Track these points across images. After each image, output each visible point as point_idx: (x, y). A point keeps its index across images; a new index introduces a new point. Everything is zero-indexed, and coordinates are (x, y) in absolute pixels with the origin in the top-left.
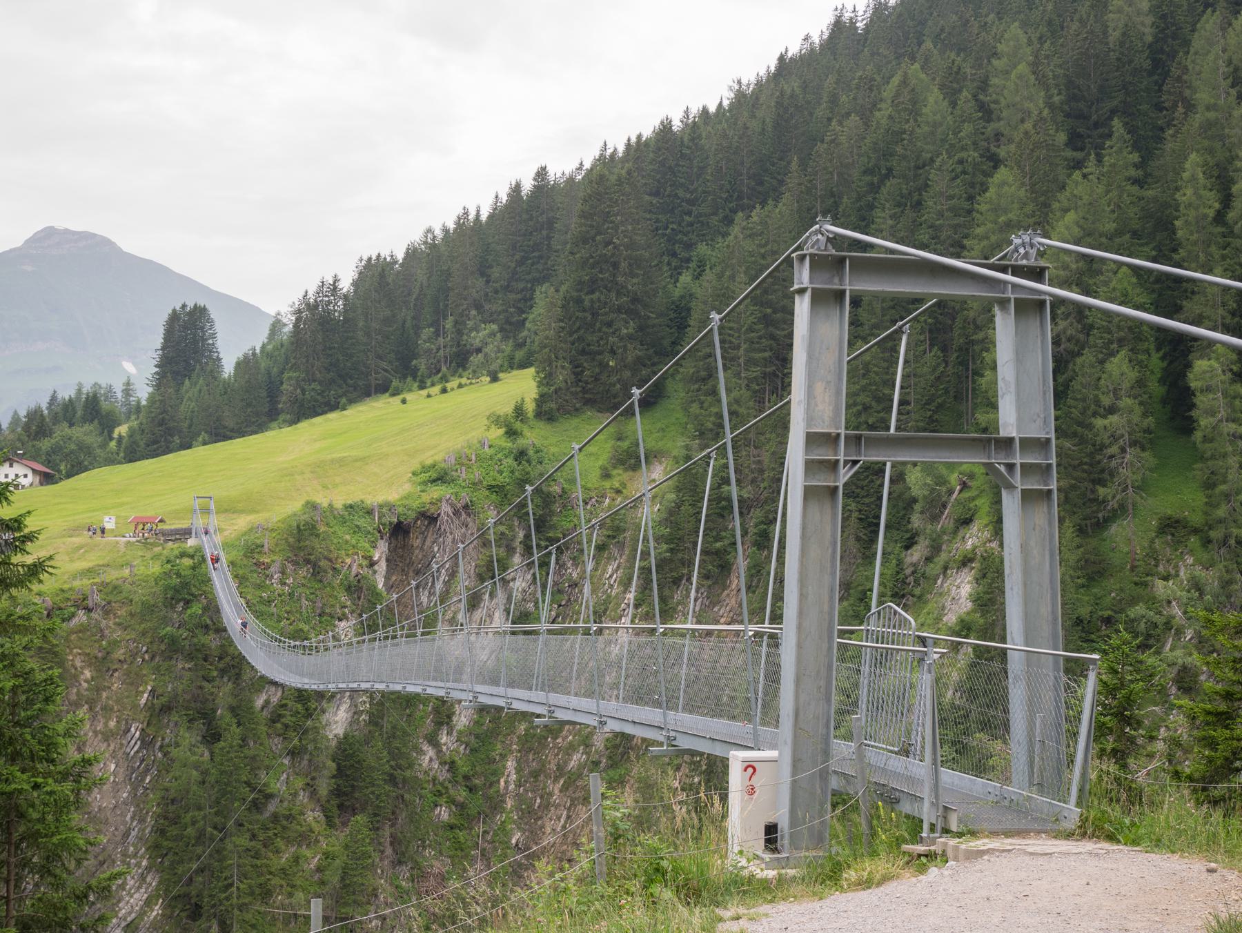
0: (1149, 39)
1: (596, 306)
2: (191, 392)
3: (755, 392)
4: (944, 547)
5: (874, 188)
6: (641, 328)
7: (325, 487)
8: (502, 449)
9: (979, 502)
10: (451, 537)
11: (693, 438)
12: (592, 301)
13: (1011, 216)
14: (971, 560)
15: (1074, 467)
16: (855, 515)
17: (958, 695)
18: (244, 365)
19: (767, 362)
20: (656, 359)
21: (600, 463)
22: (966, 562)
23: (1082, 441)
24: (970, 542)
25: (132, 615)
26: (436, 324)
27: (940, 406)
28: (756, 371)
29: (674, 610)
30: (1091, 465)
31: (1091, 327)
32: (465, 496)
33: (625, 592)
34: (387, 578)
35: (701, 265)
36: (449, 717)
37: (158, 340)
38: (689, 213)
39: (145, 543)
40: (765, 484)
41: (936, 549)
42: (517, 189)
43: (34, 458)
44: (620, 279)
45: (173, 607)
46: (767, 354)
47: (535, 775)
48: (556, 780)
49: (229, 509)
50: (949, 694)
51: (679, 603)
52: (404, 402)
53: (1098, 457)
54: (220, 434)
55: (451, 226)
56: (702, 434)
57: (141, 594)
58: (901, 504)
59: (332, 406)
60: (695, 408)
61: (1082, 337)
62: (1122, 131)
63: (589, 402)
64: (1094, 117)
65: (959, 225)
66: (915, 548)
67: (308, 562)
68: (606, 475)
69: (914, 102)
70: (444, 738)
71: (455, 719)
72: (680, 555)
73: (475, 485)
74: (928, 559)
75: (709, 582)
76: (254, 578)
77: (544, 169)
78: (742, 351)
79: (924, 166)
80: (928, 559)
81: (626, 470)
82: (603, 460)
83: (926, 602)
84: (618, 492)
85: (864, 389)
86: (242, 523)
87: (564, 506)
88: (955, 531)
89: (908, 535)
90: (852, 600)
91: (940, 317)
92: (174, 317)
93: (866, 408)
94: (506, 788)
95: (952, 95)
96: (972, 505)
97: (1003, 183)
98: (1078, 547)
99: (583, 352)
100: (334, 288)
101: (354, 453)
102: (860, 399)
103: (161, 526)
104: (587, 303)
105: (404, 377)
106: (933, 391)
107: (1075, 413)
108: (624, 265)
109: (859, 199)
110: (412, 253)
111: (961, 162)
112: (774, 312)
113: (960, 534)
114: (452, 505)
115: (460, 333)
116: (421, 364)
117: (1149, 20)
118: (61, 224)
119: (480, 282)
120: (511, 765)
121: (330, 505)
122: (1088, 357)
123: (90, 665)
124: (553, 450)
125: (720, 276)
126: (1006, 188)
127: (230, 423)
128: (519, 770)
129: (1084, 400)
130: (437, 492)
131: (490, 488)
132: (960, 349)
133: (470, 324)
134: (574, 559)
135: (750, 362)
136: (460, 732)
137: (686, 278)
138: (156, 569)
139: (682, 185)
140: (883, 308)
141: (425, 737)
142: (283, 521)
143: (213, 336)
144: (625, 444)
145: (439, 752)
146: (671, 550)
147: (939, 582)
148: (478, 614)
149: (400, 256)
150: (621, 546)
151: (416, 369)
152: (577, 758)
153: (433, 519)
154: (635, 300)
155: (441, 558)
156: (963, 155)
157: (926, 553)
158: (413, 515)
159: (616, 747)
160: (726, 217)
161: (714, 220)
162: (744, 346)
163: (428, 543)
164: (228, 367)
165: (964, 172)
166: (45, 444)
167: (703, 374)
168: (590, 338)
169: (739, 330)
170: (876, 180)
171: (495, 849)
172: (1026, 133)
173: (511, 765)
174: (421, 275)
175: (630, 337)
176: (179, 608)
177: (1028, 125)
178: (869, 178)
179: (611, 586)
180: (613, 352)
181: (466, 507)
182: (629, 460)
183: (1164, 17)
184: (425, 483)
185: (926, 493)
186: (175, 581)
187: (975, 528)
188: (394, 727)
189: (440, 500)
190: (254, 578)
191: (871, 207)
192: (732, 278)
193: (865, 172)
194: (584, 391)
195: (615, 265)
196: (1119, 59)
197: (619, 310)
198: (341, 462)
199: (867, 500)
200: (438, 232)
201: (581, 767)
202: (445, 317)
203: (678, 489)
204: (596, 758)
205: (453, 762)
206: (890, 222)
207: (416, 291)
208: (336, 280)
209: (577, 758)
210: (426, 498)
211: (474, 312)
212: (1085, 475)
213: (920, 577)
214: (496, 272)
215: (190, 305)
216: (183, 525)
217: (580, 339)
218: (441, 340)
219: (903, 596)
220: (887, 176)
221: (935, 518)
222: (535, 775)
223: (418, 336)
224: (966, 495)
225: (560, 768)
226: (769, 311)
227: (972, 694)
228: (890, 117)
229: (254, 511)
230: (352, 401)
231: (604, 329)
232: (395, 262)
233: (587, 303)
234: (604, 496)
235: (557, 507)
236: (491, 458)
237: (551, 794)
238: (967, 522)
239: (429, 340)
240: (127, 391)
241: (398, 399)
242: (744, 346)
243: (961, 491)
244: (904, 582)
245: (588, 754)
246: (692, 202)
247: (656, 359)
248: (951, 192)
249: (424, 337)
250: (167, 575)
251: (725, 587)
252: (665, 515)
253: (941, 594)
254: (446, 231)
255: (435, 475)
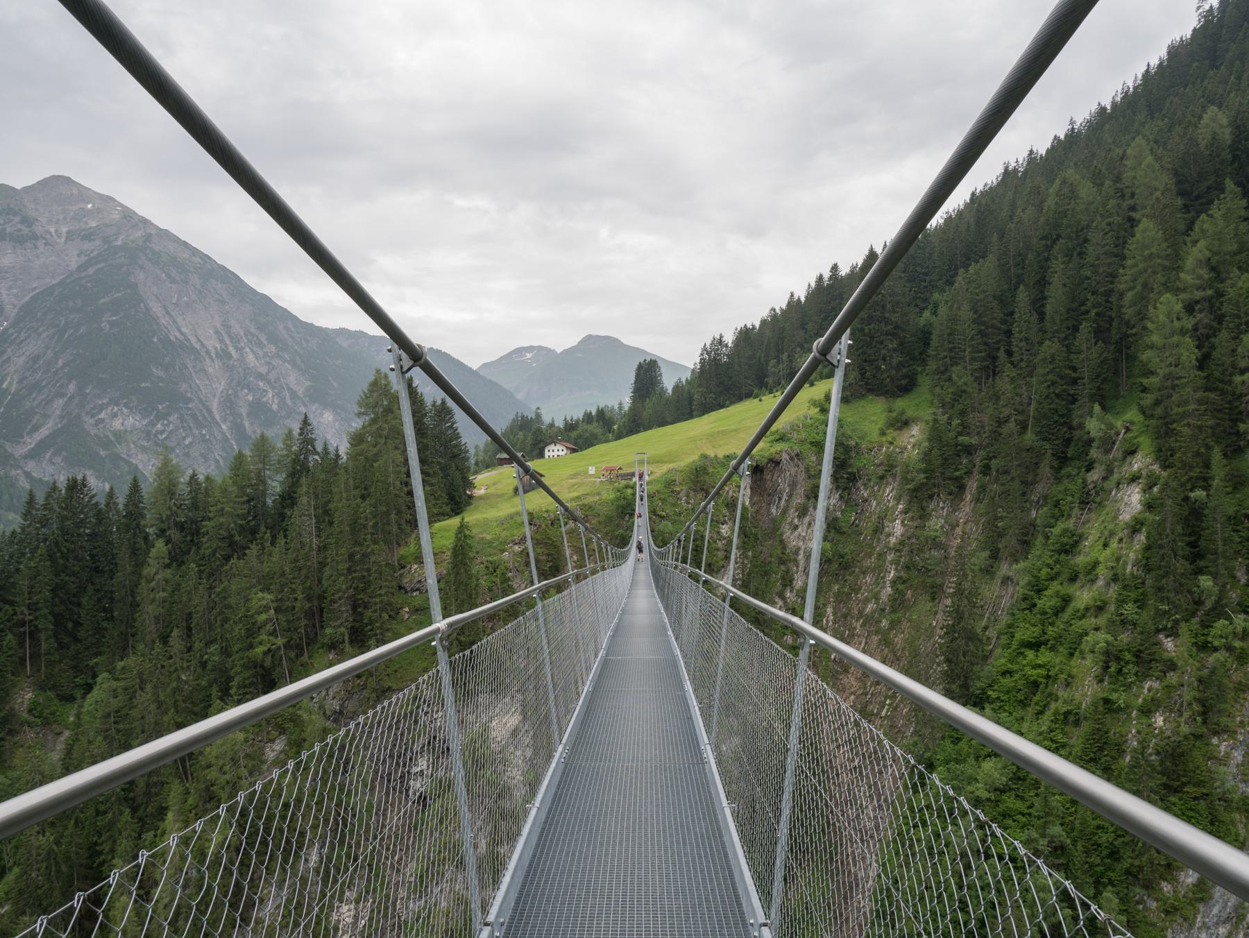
0: (1229, 142)
1: (873, 332)
2: (650, 405)
3: (977, 377)
4: (1116, 470)
5: (1048, 248)
6: (901, 344)
7: (714, 447)
8: (818, 420)
9: (1141, 439)
10: (788, 473)
11: (938, 408)
12: (870, 330)
13: (1154, 250)
14: (1139, 478)
15: (1219, 410)
16: (1050, 451)
17: (1135, 568)
18: (677, 388)
19: (983, 359)
20: (911, 362)
21: (879, 426)
22: (1134, 479)
23: (1223, 393)
24: (1136, 466)
25: (600, 523)
26: (777, 357)
27: (1105, 380)
28: (977, 365)
29: (930, 515)
30: (1230, 409)
31: (1223, 316)
32: (797, 449)
33: (898, 504)
34: (751, 499)
35: (936, 306)
36: (791, 582)
37: (632, 379)
38: (925, 281)
39: (611, 482)
40: (987, 434)
41: (1110, 471)
42: (820, 278)
43: (568, 441)
44: (887, 315)
45: (623, 519)
46: (983, 354)
47: (845, 616)
48: (857, 620)
49: (657, 461)
50: (1129, 568)
51: (933, 510)
52: (760, 400)
53: (1236, 404)
54: (663, 423)
55: (784, 307)
56: (943, 406)
57: (605, 510)
58: (1080, 444)
59: (722, 406)
60: (938, 390)
61: (1215, 324)
62: (1233, 186)
63: (870, 391)
64: (1196, 193)
65: (1110, 264)
66: (1092, 472)
67: (703, 489)
68: (883, 434)
69: (1073, 192)
70: (788, 595)
71: (794, 582)
72: (932, 481)
73: (802, 442)
74: (1105, 479)
75: (952, 497)
76: (671, 500)
77: (836, 265)
78: (967, 353)
79: (1083, 229)
80: (1105, 479)
81: (895, 430)
82: (881, 424)
83: (1104, 507)
84: (891, 443)
85: (1051, 371)
86: (665, 468)
87: (858, 453)
88: (1124, 458)
89: (1087, 464)
90: (1049, 506)
91: (1101, 323)
92: (640, 366)
93: (1053, 383)
94: (827, 624)
95: (1098, 183)
96: (1135, 441)
97: (1144, 231)
98: (1226, 466)
99: (865, 361)
100: (720, 341)
101: (733, 427)
102: (1050, 377)
103: (620, 472)
104: (866, 331)
105: (761, 388)
106: (1100, 370)
107: (1217, 374)
108: (889, 306)
109: (1038, 255)
110: (763, 322)
111: (1109, 224)
112: (987, 328)
113: (1128, 460)
114: (789, 454)
115: (791, 361)
116: (770, 380)
117: (1228, 131)
118: (594, 333)
119: (802, 332)
120: (829, 610)
121: (716, 456)
122: (1224, 335)
123: (576, 553)
124: (850, 420)
125: (951, 308)
126: (1148, 233)
127: (669, 420)
128: (834, 614)
129: (1223, 365)
130: (779, 446)
131: (811, 443)
132: (1117, 342)
133: (796, 356)
134: (865, 485)
135: (973, 359)
136: (798, 591)
137: (927, 314)
138: (612, 496)
139: (919, 264)
140: (1061, 320)
141: (777, 594)
142: (687, 466)
143: (660, 375)
144: (894, 415)
145: (785, 602)
146: (927, 478)
147: (1113, 493)
148: (807, 520)
149: (757, 326)
150: (894, 476)
151: (767, 383)
152: (870, 607)
153: (777, 463)
154: (897, 327)
155: (784, 486)
156: (1110, 220)
157: (1103, 474)
158: (765, 461)
159: (895, 600)
160: (947, 281)
161: (940, 283)
162: (968, 350)
163: (775, 477)
164: (670, 391)
165: (1112, 230)
166: (574, 434)
167: (943, 368)
168: (871, 352)
169: (965, 340)
170: (1049, 243)
171: (821, 661)
172: (1157, 199)
173: (829, 610)
174: (768, 333)
175: (894, 350)
176: (627, 518)
177: (1158, 194)
178: (1044, 242)
179: (889, 501)
180: (884, 359)
181: (797, 455)
182: (902, 423)
183: (1238, 127)
184: (772, 442)
185: (1101, 434)
186: (622, 502)
187: (1139, 456)
188: (757, 589)
189: (781, 451)
190: (671, 500)
191: (1047, 259)
192: (959, 308)
193: (1041, 239)
194: (867, 384)
195: (883, 307)
196: (1210, 155)
197: (887, 334)
198: (723, 433)
199: (1056, 442)
200: (778, 311)
201: (873, 612)
202: (782, 353)
203: (930, 440)
204: (883, 606)
205: (794, 609)
206: (1063, 266)
207: (766, 342)
208: (721, 336)
209: (870, 607)
210: (773, 450)
211: (798, 349)
212: (1227, 417)
213: (1100, 490)
214: (810, 326)
215: (648, 359)
216: (630, 470)
217: (864, 353)
218: (781, 366)
219: (1088, 503)
220: (1057, 239)
221: (1108, 451)
222: (845, 616)
223: (767, 365)
224: (1130, 435)
225: (861, 613)
226: (983, 328)
227: (1148, 568)
228: (1056, 203)
229: (673, 462)
230: (732, 403)
231: (878, 346)
232: (754, 327)
233: (866, 331)
234: (882, 446)
235: (853, 454)
236: (812, 425)
237: (855, 628)
238: (1132, 452)
239: (774, 366)
240: (620, 408)
241: (757, 400)
242: (968, 350)
243: (1125, 433)
244: (1088, 494)
245: (878, 604)
246: (926, 274)
247: (911, 362)
248: (1105, 242)
249: (771, 365)
250: (618, 499)
251: (962, 500)
252: (921, 456)
253: (1116, 501)
254: (781, 309)
255: (778, 437)
